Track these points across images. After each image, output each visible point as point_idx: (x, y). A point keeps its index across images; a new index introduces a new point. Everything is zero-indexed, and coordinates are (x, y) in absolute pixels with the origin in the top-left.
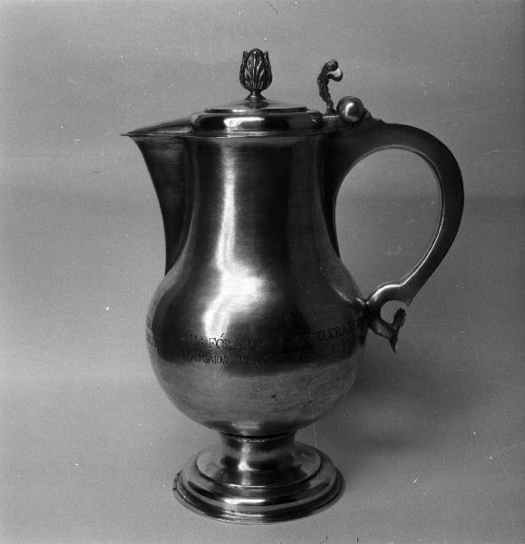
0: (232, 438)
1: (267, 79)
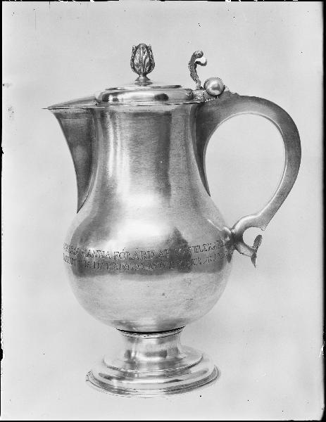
0: (132, 332)
1: (151, 65)
